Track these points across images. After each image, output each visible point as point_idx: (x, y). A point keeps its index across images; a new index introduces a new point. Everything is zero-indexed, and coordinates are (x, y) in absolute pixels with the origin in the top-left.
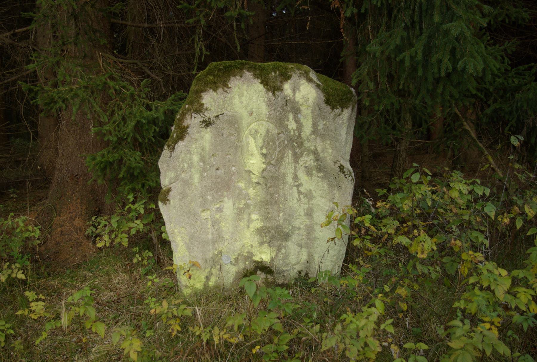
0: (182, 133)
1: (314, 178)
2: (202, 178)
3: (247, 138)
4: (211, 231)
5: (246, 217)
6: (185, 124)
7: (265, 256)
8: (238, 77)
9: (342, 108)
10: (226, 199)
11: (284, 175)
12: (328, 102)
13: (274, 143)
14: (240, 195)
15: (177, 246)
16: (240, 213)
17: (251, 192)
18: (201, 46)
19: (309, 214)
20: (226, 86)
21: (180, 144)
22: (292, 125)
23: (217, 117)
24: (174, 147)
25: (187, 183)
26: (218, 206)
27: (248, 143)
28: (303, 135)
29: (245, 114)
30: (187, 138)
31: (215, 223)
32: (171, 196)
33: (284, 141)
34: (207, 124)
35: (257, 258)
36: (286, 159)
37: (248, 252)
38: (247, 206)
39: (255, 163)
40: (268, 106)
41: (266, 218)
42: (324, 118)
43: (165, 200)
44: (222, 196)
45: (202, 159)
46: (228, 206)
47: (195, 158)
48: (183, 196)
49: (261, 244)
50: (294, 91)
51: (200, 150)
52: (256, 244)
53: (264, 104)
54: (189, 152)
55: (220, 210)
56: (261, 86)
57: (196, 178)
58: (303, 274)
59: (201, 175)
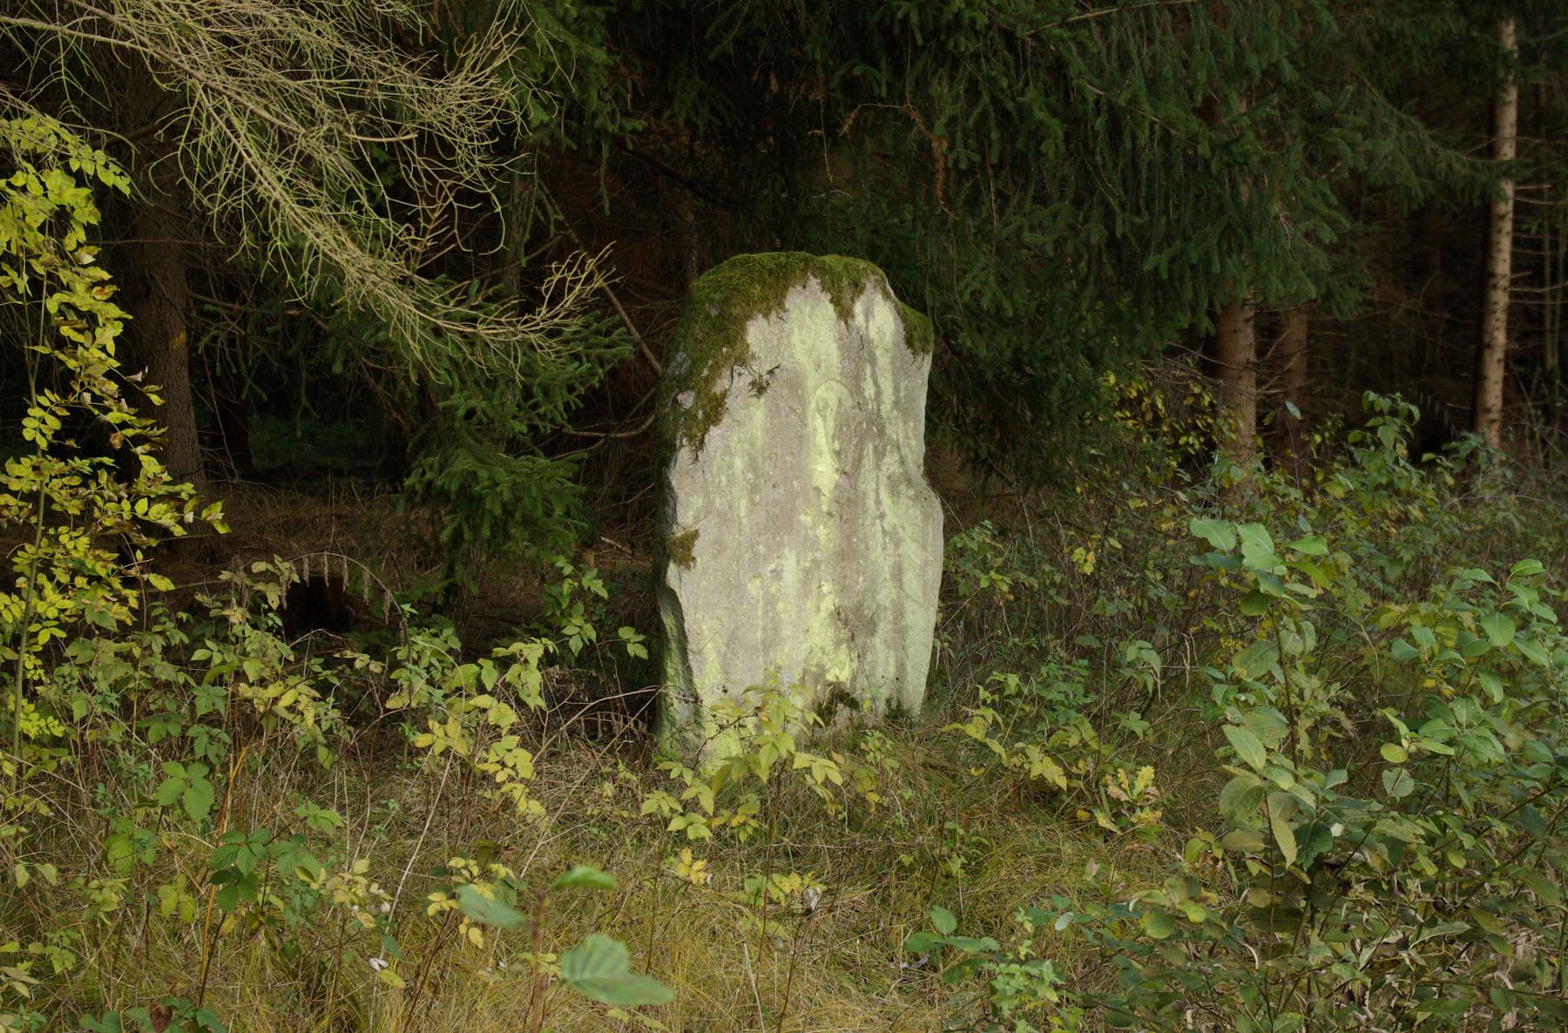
0: (715, 410)
1: (903, 500)
2: (753, 504)
3: (813, 418)
4: (760, 622)
5: (814, 586)
6: (717, 389)
7: (841, 671)
8: (799, 288)
9: (730, 342)
10: (786, 551)
11: (864, 494)
12: (909, 341)
13: (849, 427)
14: (809, 544)
15: (703, 662)
16: (808, 576)
17: (822, 531)
18: (106, 103)
19: (898, 574)
20: (781, 305)
21: (714, 432)
22: (870, 391)
23: (771, 372)
24: (702, 441)
25: (725, 519)
26: (773, 566)
27: (815, 430)
28: (883, 413)
29: (810, 368)
30: (726, 419)
31: (771, 601)
32: (698, 549)
33: (860, 423)
34: (760, 388)
35: (830, 677)
36: (865, 461)
37: (818, 665)
38: (816, 563)
39: (824, 471)
40: (840, 348)
41: (843, 589)
42: (907, 375)
43: (686, 560)
44: (781, 544)
45: (753, 465)
46: (791, 565)
47: (739, 463)
48: (719, 547)
49: (838, 644)
50: (867, 321)
51: (747, 446)
52: (830, 647)
53: (834, 346)
54: (727, 450)
55: (777, 574)
56: (831, 307)
57: (743, 506)
58: (894, 705)
59: (751, 500)
